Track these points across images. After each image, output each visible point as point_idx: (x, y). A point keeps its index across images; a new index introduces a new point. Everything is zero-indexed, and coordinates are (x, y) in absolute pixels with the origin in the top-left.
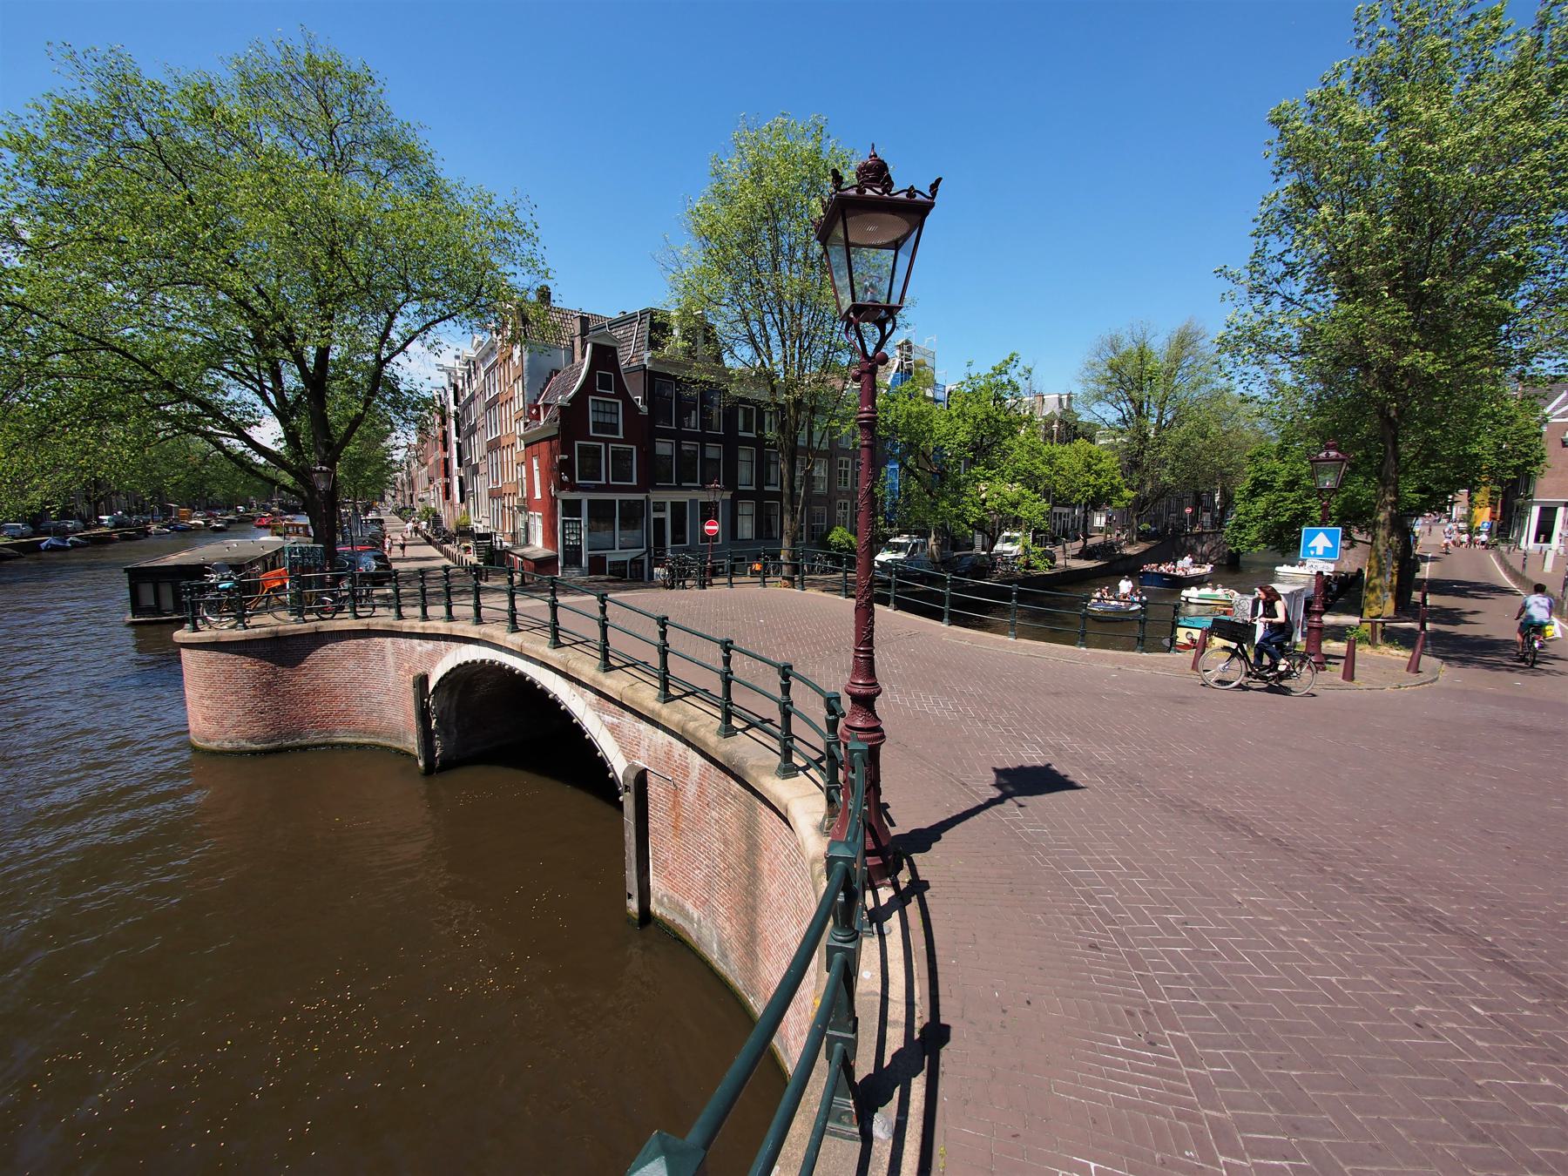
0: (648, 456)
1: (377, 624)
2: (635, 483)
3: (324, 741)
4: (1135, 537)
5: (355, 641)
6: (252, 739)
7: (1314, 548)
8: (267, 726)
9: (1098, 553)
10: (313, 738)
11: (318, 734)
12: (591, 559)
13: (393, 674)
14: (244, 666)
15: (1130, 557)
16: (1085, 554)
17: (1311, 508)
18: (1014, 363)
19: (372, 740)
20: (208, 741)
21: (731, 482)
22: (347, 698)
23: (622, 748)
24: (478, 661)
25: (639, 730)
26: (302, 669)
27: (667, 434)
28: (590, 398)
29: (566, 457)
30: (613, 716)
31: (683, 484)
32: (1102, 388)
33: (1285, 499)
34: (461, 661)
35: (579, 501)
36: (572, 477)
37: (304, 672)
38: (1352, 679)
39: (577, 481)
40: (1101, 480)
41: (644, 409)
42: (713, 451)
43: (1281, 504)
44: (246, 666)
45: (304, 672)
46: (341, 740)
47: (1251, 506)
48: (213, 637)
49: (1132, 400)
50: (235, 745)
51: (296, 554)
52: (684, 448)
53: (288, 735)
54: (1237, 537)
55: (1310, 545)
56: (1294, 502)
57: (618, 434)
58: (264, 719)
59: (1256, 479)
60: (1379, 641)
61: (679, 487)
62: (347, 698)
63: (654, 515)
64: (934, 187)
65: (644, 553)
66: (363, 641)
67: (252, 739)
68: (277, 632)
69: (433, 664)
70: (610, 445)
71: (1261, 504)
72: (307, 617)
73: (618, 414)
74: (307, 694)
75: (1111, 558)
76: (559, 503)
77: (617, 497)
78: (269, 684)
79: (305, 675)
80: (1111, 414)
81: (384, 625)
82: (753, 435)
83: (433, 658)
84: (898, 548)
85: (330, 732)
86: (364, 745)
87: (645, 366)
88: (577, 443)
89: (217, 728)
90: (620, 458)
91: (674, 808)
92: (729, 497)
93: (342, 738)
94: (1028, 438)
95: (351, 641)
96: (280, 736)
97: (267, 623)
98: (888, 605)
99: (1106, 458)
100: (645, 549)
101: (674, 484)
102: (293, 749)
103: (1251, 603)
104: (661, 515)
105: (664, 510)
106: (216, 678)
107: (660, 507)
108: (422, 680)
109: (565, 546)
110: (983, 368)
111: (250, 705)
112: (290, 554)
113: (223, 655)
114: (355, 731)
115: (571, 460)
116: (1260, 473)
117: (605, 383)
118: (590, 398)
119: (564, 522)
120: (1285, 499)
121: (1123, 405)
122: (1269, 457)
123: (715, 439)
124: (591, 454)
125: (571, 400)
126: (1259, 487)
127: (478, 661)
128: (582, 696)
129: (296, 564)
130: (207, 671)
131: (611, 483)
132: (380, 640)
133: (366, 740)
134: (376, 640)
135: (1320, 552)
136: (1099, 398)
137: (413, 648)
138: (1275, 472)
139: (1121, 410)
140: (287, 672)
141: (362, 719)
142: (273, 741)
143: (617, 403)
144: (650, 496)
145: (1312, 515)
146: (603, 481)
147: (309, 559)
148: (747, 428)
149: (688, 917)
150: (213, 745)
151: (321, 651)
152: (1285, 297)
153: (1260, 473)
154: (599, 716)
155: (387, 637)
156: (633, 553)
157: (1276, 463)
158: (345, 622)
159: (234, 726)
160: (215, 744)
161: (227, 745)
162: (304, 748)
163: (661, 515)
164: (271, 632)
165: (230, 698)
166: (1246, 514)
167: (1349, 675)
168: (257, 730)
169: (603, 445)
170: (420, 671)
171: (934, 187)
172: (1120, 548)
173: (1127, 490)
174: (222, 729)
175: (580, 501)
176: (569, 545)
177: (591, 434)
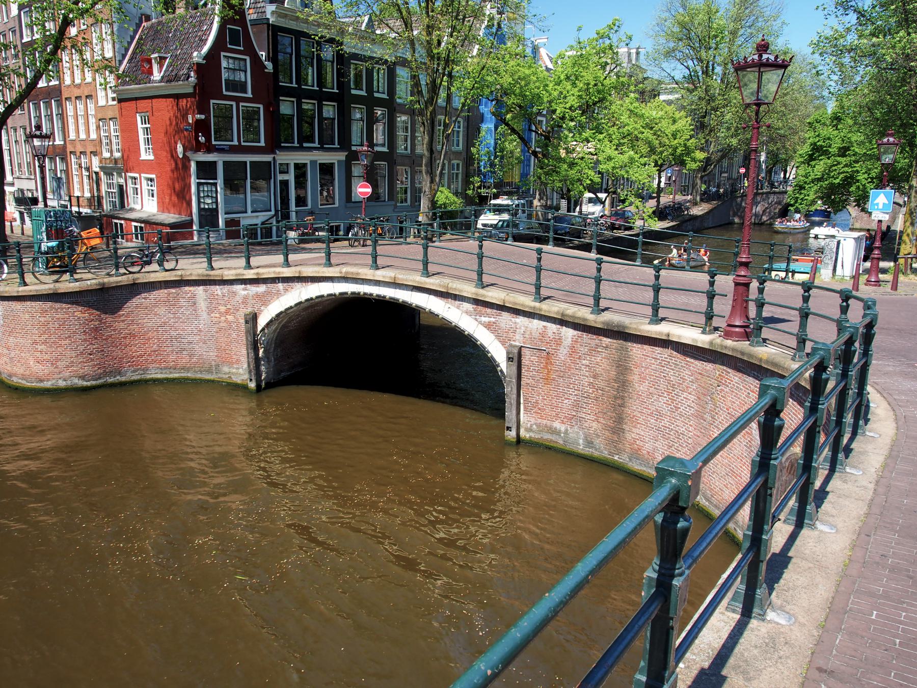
0: (274, 118)
1: (191, 274)
2: (262, 144)
3: (139, 377)
4: (698, 198)
5: (166, 291)
6: (82, 377)
7: (877, 205)
8: (95, 365)
9: (670, 215)
10: (131, 376)
11: (134, 371)
12: (229, 223)
13: (204, 315)
14: (76, 314)
15: (695, 218)
16: (660, 214)
17: (858, 172)
18: (615, 28)
19: (182, 375)
20: (42, 381)
21: (345, 143)
22: (159, 339)
23: (498, 337)
24: (362, 293)
25: (515, 323)
26: (120, 316)
27: (289, 92)
28: (223, 54)
29: (203, 117)
30: (489, 316)
31: (305, 145)
32: (672, 45)
33: (839, 163)
34: (303, 299)
35: (214, 164)
36: (208, 139)
37: (122, 318)
38: (896, 289)
39: (214, 143)
40: (676, 141)
41: (269, 66)
42: (329, 110)
43: (836, 168)
44: (78, 313)
45: (122, 318)
46: (151, 376)
47: (810, 169)
48: (50, 289)
49: (700, 60)
50: (69, 383)
51: (51, 217)
52: (305, 107)
53: (110, 374)
54: (798, 198)
55: (875, 202)
56: (846, 166)
57: (246, 92)
58: (92, 360)
59: (815, 144)
60: (909, 271)
61: (301, 148)
62: (159, 339)
63: (280, 177)
64: (791, 59)
65: (272, 217)
66: (173, 291)
67: (82, 377)
68: (104, 284)
69: (265, 304)
70: (241, 104)
71: (820, 167)
72: (130, 269)
73: (246, 72)
74: (125, 338)
75: (680, 218)
76: (193, 166)
77: (248, 158)
78: (96, 329)
79: (123, 321)
80: (680, 72)
81: (199, 275)
82: (363, 93)
83: (264, 300)
84: (499, 210)
85: (143, 370)
86: (174, 379)
87: (268, 19)
88: (212, 101)
89: (52, 369)
90: (251, 117)
91: (546, 367)
92: (344, 158)
93: (154, 374)
94: (631, 104)
95: (162, 291)
96: (105, 374)
97: (88, 279)
98: (590, 252)
99: (680, 118)
100: (273, 213)
101: (296, 144)
102: (112, 385)
103: (836, 243)
104: (284, 177)
105: (287, 172)
106: (51, 325)
107: (284, 170)
108: (253, 319)
109: (200, 210)
110: (589, 34)
111: (81, 348)
112: (46, 217)
113: (58, 305)
114: (166, 368)
115: (208, 119)
116: (817, 139)
117: (235, 40)
118: (223, 54)
119: (199, 184)
120: (839, 163)
121: (690, 63)
122: (824, 124)
123: (331, 97)
124: (225, 116)
125: (206, 57)
126: (818, 151)
127: (337, 293)
128: (458, 307)
129: (51, 226)
130: (42, 319)
131: (243, 144)
132: (192, 288)
133: (176, 375)
134: (187, 288)
135: (881, 207)
136: (669, 54)
137: (235, 293)
138: (829, 139)
139: (688, 68)
140: (109, 318)
141: (172, 357)
142: (100, 378)
143: (245, 60)
144: (277, 158)
145: (858, 178)
146: (236, 143)
147: (61, 221)
148: (358, 86)
149: (557, 432)
150: (48, 384)
151: (136, 301)
152: (859, 12)
153: (817, 139)
154: (476, 320)
155: (199, 285)
156: (262, 217)
157: (830, 129)
158: (153, 273)
159: (67, 367)
160: (50, 383)
161: (62, 384)
162: (122, 384)
163: (284, 177)
164: (100, 284)
165: (63, 342)
166: (806, 176)
167: (895, 287)
168: (87, 369)
169: (234, 104)
170: (250, 310)
171: (791, 59)
172: (688, 209)
173: (698, 152)
174: (56, 370)
175: (215, 162)
176: (204, 209)
177: (225, 93)
